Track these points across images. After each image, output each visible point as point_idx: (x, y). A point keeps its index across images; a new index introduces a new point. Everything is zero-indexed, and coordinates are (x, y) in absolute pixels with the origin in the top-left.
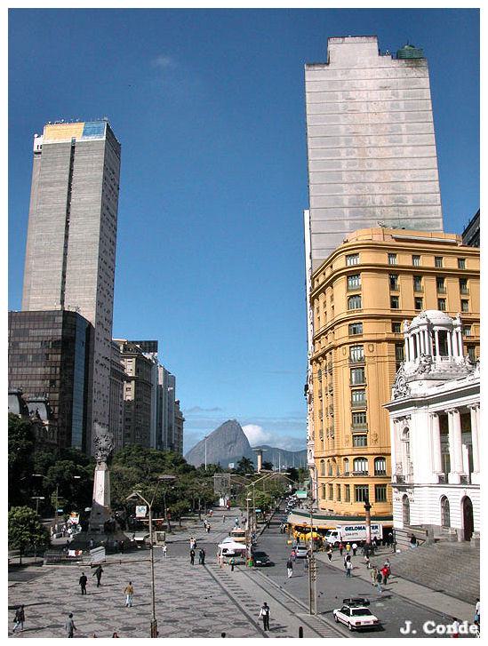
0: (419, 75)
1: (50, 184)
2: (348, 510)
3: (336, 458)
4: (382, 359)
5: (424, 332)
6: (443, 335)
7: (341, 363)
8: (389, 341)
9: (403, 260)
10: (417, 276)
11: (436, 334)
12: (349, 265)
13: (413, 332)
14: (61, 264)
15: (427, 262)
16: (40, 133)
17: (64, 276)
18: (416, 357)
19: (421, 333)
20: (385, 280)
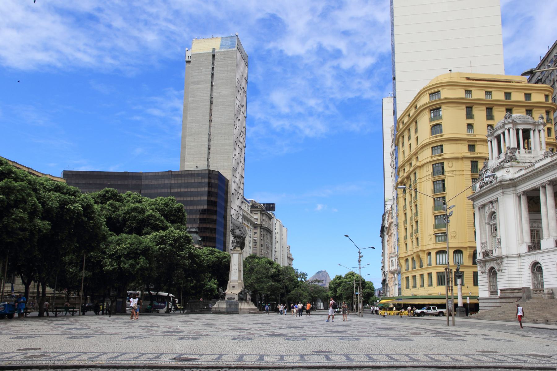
1: (198, 83)
5: (509, 130)
7: (425, 179)
12: (432, 100)
13: (496, 134)
14: (207, 140)
15: (498, 96)
18: (500, 152)
20: (463, 112)
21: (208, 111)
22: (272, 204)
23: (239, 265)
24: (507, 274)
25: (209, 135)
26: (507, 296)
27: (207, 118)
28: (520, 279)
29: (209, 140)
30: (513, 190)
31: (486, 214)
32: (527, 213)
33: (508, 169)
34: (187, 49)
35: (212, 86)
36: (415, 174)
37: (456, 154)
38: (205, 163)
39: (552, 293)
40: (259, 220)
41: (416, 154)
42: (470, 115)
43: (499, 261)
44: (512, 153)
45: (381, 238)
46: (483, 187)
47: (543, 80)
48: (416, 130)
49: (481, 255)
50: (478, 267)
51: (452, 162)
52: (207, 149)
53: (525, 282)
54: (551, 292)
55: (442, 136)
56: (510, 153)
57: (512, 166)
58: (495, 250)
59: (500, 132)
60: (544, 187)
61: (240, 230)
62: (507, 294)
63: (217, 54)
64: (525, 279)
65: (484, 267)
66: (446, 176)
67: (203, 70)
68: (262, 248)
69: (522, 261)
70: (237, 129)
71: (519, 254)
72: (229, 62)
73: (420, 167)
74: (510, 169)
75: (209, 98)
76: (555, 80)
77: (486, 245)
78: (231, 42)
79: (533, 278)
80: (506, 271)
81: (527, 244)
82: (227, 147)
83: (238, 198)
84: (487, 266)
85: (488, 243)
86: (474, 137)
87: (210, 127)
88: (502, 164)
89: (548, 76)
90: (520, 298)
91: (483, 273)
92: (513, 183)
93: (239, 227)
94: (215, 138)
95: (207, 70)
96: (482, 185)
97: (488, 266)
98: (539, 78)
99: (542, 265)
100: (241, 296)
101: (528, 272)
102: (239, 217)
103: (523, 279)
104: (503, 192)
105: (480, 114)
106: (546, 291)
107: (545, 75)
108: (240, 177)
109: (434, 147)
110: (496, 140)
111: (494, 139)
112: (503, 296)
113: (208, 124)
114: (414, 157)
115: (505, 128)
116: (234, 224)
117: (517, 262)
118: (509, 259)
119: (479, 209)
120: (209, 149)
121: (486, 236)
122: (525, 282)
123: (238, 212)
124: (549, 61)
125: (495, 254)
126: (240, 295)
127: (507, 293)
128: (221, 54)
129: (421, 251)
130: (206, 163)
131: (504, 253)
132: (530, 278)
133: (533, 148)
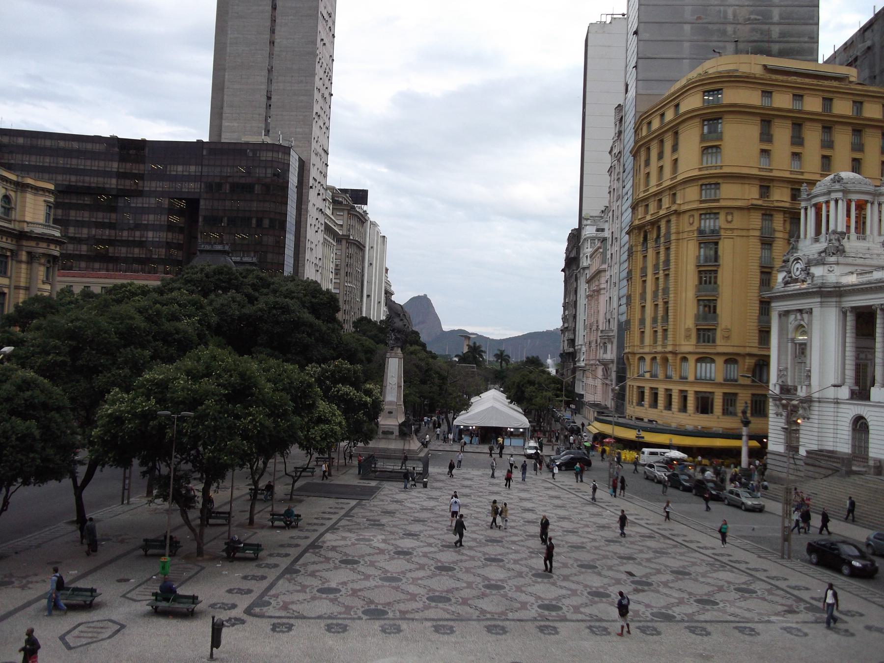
3: (629, 355)
5: (836, 201)
6: (861, 206)
8: (752, 208)
9: (782, 101)
10: (858, 129)
13: (814, 201)
15: (813, 104)
18: (818, 232)
19: (832, 204)
23: (399, 378)
25: (270, 71)
30: (836, 302)
31: (790, 326)
36: (669, 221)
38: (261, 125)
40: (345, 228)
41: (671, 188)
42: (766, 136)
45: (563, 273)
46: (790, 283)
48: (675, 148)
49: (778, 388)
52: (264, 99)
57: (838, 264)
59: (822, 199)
69: (840, 410)
71: (837, 399)
73: (676, 213)
74: (835, 267)
79: (854, 439)
83: (319, 194)
88: (823, 255)
92: (837, 291)
99: (868, 420)
102: (318, 228)
104: (821, 302)
105: (782, 134)
106: (871, 463)
110: (813, 209)
114: (667, 193)
117: (832, 410)
118: (822, 405)
119: (780, 316)
120: (269, 98)
121: (787, 360)
126: (402, 427)
133: (868, 232)
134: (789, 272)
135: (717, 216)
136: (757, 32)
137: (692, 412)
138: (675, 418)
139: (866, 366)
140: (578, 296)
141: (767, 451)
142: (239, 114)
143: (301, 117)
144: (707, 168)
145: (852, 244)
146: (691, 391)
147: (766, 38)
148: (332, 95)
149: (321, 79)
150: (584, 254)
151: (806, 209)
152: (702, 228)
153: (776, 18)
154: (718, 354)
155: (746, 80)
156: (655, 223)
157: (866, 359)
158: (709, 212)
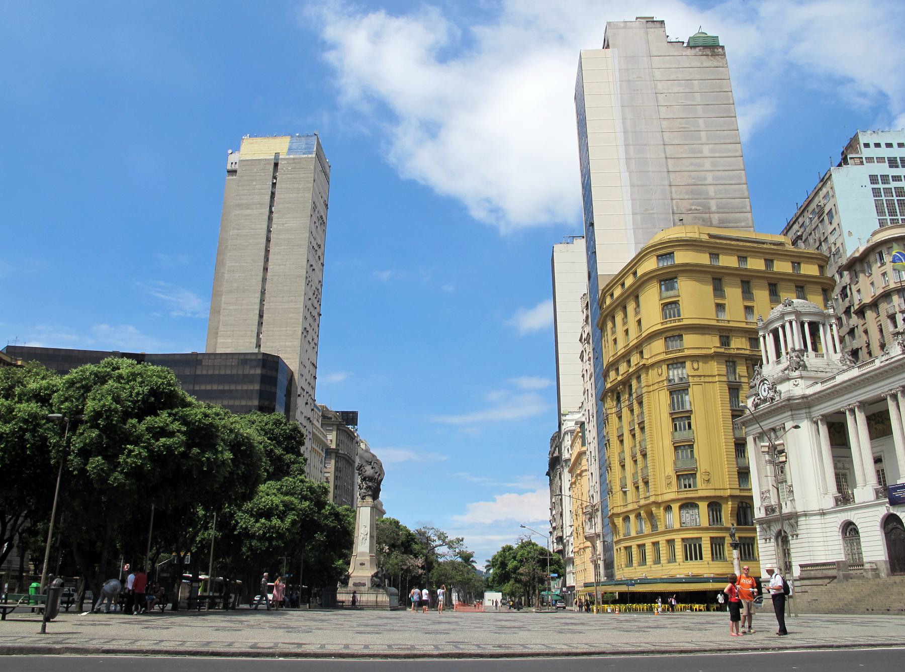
0: (716, 64)
1: (248, 207)
2: (673, 573)
4: (710, 379)
5: (791, 323)
6: (814, 327)
7: (656, 387)
8: (716, 356)
9: (728, 261)
10: (747, 282)
11: (806, 326)
14: (258, 301)
15: (756, 264)
16: (237, 149)
17: (261, 316)
18: (778, 354)
19: (787, 326)
21: (263, 253)
22: (353, 412)
24: (806, 540)
26: (813, 576)
27: (260, 264)
28: (826, 548)
29: (262, 301)
32: (830, 447)
33: (796, 381)
34: (230, 151)
35: (271, 212)
37: (703, 350)
38: (253, 340)
39: (876, 569)
43: (792, 521)
44: (800, 358)
46: (759, 405)
47: (804, 238)
48: (637, 313)
49: (763, 510)
50: (758, 530)
51: (698, 361)
53: (834, 552)
54: (875, 567)
55: (680, 320)
56: (796, 357)
58: (786, 504)
59: (777, 324)
60: (852, 411)
61: (372, 468)
62: (812, 572)
63: (283, 163)
64: (834, 548)
65: (768, 531)
66: (691, 384)
67: (257, 186)
68: (338, 492)
70: (310, 284)
72: (302, 175)
73: (646, 368)
75: (265, 232)
76: (822, 240)
77: (768, 495)
78: (306, 144)
80: (805, 536)
81: (833, 494)
82: (291, 315)
83: (307, 403)
84: (772, 528)
85: (771, 492)
86: (729, 325)
87: (264, 280)
88: (786, 372)
89: (811, 233)
90: (835, 577)
91: (766, 540)
92: (805, 402)
93: (371, 462)
94: (272, 299)
95: (264, 186)
96: (757, 403)
97: (775, 528)
98: (799, 234)
100: (376, 579)
101: (837, 538)
103: (830, 548)
104: (792, 415)
106: (867, 566)
107: (807, 231)
108: (311, 366)
109: (670, 337)
110: (771, 335)
111: (769, 334)
112: (805, 575)
113: (262, 274)
115: (786, 319)
116: (361, 458)
117: (819, 521)
122: (834, 552)
123: (305, 427)
124: (809, 212)
125: (786, 510)
126: (374, 578)
127: (812, 570)
128: (288, 163)
129: (654, 503)
130: (254, 341)
131: (799, 509)
132: (842, 547)
134: (757, 395)
135: (683, 365)
136: (699, 220)
137: (681, 560)
138: (666, 570)
139: (845, 475)
140: (563, 482)
141: (761, 580)
142: (233, 331)
143: (291, 332)
144: (671, 352)
145: (810, 359)
146: (678, 537)
147: (707, 211)
148: (320, 315)
149: (310, 299)
150: (565, 447)
151: (764, 337)
152: (671, 377)
153: (714, 208)
154: (701, 498)
155: (694, 243)
156: (626, 383)
157: (844, 469)
158: (675, 361)
